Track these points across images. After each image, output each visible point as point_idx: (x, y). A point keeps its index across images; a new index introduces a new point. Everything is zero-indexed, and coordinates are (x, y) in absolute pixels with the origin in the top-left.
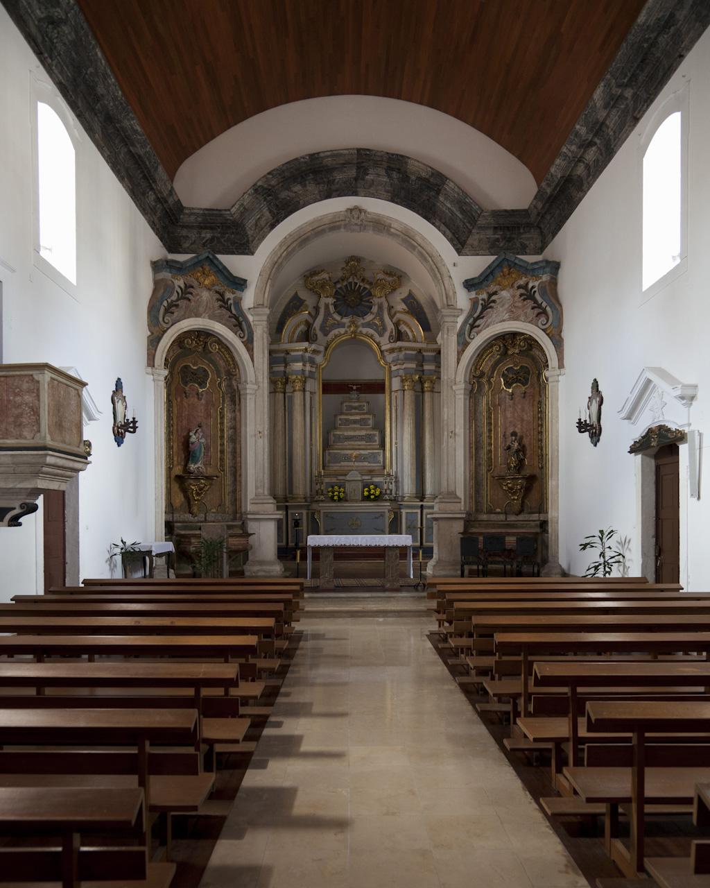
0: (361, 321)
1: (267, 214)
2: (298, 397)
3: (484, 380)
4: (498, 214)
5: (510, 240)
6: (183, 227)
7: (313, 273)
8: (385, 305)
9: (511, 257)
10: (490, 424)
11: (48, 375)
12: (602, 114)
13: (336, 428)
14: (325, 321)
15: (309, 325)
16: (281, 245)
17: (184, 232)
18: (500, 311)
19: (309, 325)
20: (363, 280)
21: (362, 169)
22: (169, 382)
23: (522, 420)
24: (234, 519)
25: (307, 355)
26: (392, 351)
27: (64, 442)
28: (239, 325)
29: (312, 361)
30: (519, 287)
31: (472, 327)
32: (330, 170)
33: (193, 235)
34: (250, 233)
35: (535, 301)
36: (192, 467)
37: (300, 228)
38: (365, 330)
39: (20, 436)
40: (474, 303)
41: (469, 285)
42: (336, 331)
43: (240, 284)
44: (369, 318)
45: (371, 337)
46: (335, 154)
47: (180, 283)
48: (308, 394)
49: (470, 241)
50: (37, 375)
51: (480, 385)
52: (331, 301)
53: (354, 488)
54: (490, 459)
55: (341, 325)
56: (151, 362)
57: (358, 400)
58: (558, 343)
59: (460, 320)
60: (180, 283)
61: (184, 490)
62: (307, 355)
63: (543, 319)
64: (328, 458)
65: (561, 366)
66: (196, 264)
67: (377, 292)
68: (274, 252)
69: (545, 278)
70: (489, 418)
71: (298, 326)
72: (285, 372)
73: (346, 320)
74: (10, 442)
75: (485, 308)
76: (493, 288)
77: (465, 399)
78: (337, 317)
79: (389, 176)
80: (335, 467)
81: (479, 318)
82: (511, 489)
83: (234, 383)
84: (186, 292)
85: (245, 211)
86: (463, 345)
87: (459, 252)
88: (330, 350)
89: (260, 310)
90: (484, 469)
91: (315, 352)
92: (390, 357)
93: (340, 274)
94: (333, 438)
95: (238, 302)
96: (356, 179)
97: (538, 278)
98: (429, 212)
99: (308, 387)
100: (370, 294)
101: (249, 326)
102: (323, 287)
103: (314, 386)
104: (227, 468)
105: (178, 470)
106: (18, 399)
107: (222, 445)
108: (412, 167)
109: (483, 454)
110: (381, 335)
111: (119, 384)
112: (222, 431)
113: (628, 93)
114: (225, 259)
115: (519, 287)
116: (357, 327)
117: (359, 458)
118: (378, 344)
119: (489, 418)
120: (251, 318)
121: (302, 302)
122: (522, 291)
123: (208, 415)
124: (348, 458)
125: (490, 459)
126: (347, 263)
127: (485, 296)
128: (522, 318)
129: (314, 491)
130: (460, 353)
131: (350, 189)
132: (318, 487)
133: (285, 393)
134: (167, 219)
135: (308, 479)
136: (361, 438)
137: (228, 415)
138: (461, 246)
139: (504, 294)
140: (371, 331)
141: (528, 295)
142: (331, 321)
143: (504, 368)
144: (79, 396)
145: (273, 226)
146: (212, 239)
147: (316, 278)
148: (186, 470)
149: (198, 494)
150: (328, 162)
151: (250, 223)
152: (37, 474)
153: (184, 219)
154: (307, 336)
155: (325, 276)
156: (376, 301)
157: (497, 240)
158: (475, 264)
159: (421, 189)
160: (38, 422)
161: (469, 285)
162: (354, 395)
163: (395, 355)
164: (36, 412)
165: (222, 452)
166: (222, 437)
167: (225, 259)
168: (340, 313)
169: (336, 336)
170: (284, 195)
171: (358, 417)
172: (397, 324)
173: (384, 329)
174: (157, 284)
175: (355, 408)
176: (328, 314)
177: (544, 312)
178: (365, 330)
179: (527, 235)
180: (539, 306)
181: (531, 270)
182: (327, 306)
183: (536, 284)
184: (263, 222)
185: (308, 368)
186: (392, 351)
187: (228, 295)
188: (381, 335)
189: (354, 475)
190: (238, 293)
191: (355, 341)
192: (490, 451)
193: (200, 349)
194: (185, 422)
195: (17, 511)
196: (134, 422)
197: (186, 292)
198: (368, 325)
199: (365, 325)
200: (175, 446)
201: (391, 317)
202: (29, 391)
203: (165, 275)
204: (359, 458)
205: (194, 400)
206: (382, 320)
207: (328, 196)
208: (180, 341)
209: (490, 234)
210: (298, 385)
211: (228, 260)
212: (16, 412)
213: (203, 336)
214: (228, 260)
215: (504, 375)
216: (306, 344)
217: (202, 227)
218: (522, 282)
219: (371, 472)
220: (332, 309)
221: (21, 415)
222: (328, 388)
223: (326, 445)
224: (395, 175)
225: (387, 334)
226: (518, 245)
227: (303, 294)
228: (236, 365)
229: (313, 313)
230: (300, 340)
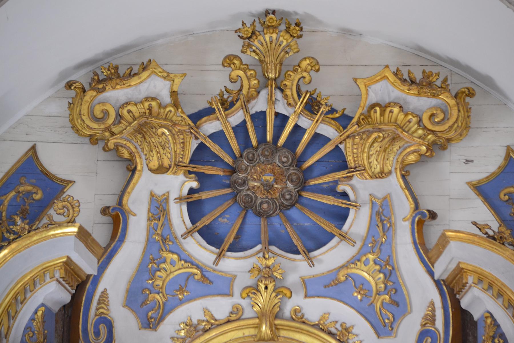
0: (297, 269)
8: (403, 207)
20: (312, 107)
38: (315, 308)
42: (193, 310)
44: (332, 256)
52: (177, 184)
55: (209, 283)
93: (217, 81)
100: (338, 162)
102: (143, 130)
121: (54, 188)
142: (172, 270)
147: (116, 94)
155: (156, 86)
156: (361, 188)
168: (211, 236)
172: (451, 288)
173: (398, 302)
176: (161, 239)
178: (315, 308)
182: (159, 208)
198: (331, 286)
199: (311, 288)
201: (427, 255)
206: (389, 270)
220: (179, 217)
227: (62, 158)
229: (101, 234)
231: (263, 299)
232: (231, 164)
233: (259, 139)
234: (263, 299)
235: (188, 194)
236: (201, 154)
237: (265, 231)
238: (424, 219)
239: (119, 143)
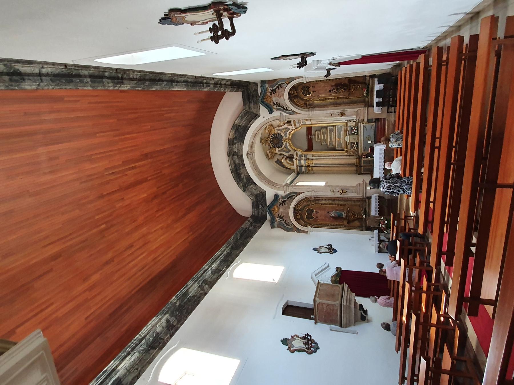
0: (284, 137)
1: (252, 186)
2: (314, 162)
3: (308, 103)
4: (244, 104)
5: (253, 96)
6: (258, 214)
7: (267, 156)
8: (277, 128)
9: (260, 99)
10: (326, 99)
11: (317, 299)
12: (212, 86)
13: (327, 144)
14: (284, 151)
15: (287, 157)
16: (262, 181)
17: (260, 214)
18: (281, 101)
19: (287, 157)
20: (269, 137)
21: (235, 154)
22: (313, 226)
23: (324, 86)
24: (365, 201)
25: (298, 158)
26: (295, 125)
27: (338, 294)
28: (291, 197)
29: (300, 156)
30: (271, 95)
31: (287, 110)
32: (235, 165)
33: (261, 211)
34: (258, 192)
35: (276, 88)
36: (344, 216)
37: (256, 174)
38: (288, 136)
39: (337, 310)
40: (277, 109)
41: (271, 112)
42: (289, 147)
43: (276, 196)
44: (283, 134)
45: (290, 133)
46: (230, 164)
47: (278, 219)
48: (313, 158)
49: (255, 112)
50: (317, 303)
51: (309, 105)
52: (277, 149)
53: (353, 139)
54: (341, 98)
55: (286, 146)
56: (306, 232)
57: (315, 135)
58: (293, 79)
59: (284, 114)
60: (278, 219)
61: (354, 220)
62: (298, 158)
63: (283, 85)
64: (339, 149)
65: (302, 77)
66: (271, 213)
67: (273, 132)
68: (265, 184)
69: (267, 86)
70: (323, 100)
71: (287, 162)
72: (305, 166)
73: (284, 143)
74: (339, 313)
75: (279, 106)
76: (272, 104)
77: (316, 111)
78: (283, 147)
79: (235, 144)
80: (343, 145)
81: (283, 107)
82: (354, 90)
83: (312, 199)
84: (281, 217)
85: (252, 194)
86: (294, 112)
87: (259, 116)
88: (296, 149)
89: (285, 189)
90: (346, 100)
91: (297, 156)
92: (298, 125)
93: (267, 146)
94: (331, 146)
95: (283, 197)
96: (237, 155)
97: (267, 89)
98: (246, 129)
99: (311, 158)
100: (274, 134)
101: (290, 193)
102: (272, 153)
103: (310, 155)
104: (345, 203)
105: (345, 223)
106: (325, 309)
107: (335, 204)
108: (231, 136)
109: (338, 101)
110: (289, 129)
111: (315, 249)
112: (330, 204)
113: (205, 81)
114: (268, 204)
115: (271, 95)
116: (286, 139)
117: (339, 137)
118: (293, 130)
119: (323, 100)
120: (288, 192)
121: (278, 160)
122: (272, 94)
123: (324, 209)
124: (339, 141)
125: (341, 98)
126: (263, 144)
127: (275, 106)
128: (283, 93)
129: (354, 154)
130: (297, 113)
131: (241, 157)
132: (352, 153)
133: (313, 166)
134: (258, 220)
135: (348, 157)
136: (331, 134)
137: (324, 202)
138: (256, 116)
139: (274, 100)
140: (288, 133)
141: (274, 91)
142: (285, 149)
143: (302, 96)
144: (323, 284)
145: (256, 184)
146: (262, 205)
147: (269, 155)
148: (345, 219)
149: (355, 215)
150: (233, 166)
151: (256, 192)
152: (349, 307)
153: (256, 214)
154: (291, 158)
155: (268, 151)
156: (276, 132)
157: (253, 101)
158: (263, 111)
159: (239, 132)
160: (332, 305)
161: (271, 112)
162: (313, 137)
163: (296, 124)
164: (329, 305)
165: (338, 205)
166: (332, 204)
167: (268, 204)
168: (282, 146)
169: (290, 147)
170: (245, 181)
171: (322, 136)
172: (285, 124)
173: (287, 128)
174: (278, 227)
175: (318, 136)
176: (282, 150)
177: (280, 85)
178: (288, 136)
179: (251, 89)
180: (278, 87)
181: (264, 91)
182: (279, 151)
183: (269, 89)
184: (254, 188)
185: (303, 158)
186: (295, 125)
187: (280, 201)
188: (289, 129)
189: (347, 139)
190: (280, 197)
191: (292, 139)
192: (337, 98)
193: (300, 212)
194: (327, 219)
195: (362, 312)
196: (328, 245)
197: (281, 217)
198: (285, 134)
199: (286, 136)
200: (336, 223)
201: (281, 126)
202: (322, 305)
203: (275, 224)
204: (339, 137)
205: (318, 215)
206: (283, 129)
207: (244, 165)
208: (297, 220)
209: (251, 105)
210: (310, 162)
211: (269, 201)
212: (329, 310)
213: (295, 211)
214: (269, 201)
215: (306, 95)
216: (294, 160)
217: (258, 208)
218: (269, 94)
219: (346, 131)
220: (280, 149)
221: (330, 309)
222: (310, 148)
223: (334, 149)
224: (235, 142)
225: (289, 127)
226: (254, 93)
227: (276, 160)
228: (305, 198)
229: (282, 156)
230: (293, 161)
231: (287, 141)
232: (485, 306)
233: (272, 142)
234: (287, 141)
235: (224, 93)
236: (274, 147)
237: (51, 172)
238: (279, 126)
239: (274, 155)
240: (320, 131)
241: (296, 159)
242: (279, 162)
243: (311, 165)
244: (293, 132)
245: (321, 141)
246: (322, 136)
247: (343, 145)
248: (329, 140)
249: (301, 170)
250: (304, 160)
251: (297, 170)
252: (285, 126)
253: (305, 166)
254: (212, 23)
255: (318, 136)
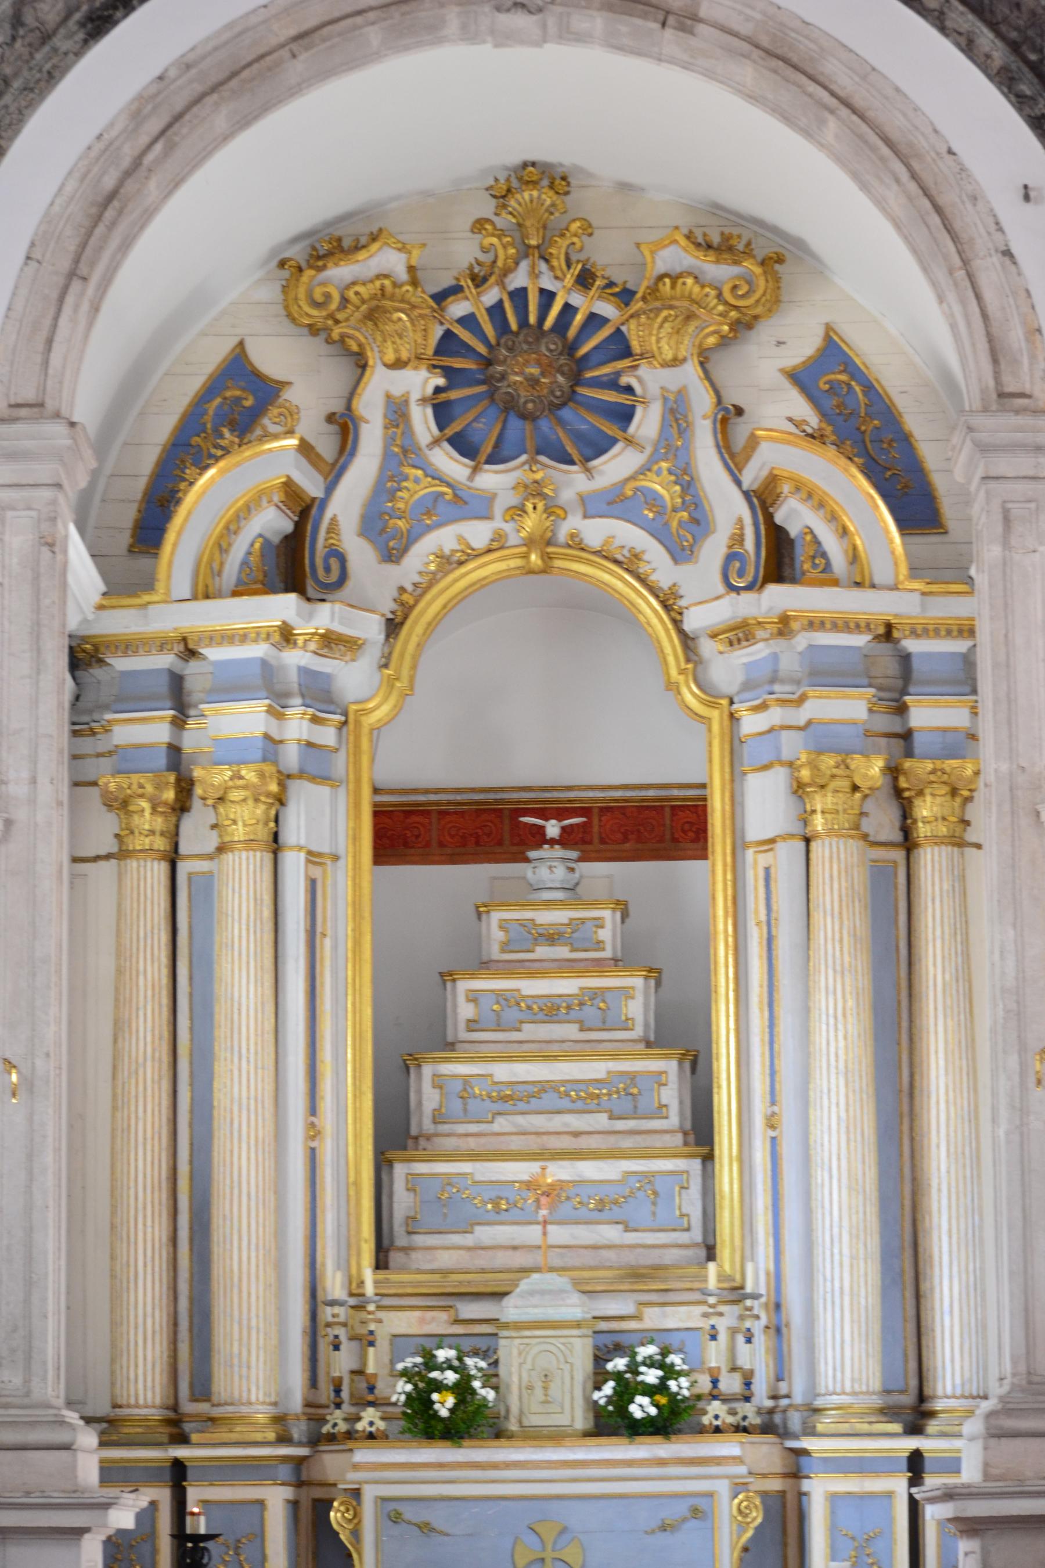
0: (573, 483)
2: (242, 877)
7: (328, 246)
8: (702, 402)
15: (304, 511)
20: (585, 280)
25: (295, 658)
26: (740, 633)
38: (596, 531)
42: (445, 538)
44: (616, 466)
45: (631, 564)
48: (294, 864)
52: (419, 382)
53: (545, 1372)
55: (463, 504)
62: (295, 658)
64: (402, 1202)
72: (174, 750)
73: (494, 480)
78: (450, 464)
80: (440, 1254)
91: (331, 642)
92: (727, 667)
93: (465, 252)
99: (294, 831)
100: (620, 347)
103: (328, 821)
110: (681, 552)
126: (503, 196)
136: (584, 1097)
140: (628, 535)
142: (416, 488)
154: (293, 564)
155: (388, 260)
156: (649, 380)
168: (464, 446)
169: (448, 562)
171: (567, 986)
172: (763, 500)
175: (552, 938)
176: (401, 452)
178: (596, 531)
182: (397, 413)
185: (297, 726)
186: (740, 633)
188: (681, 552)
198: (615, 502)
199: (589, 507)
201: (734, 459)
206: (687, 480)
210: (245, 818)
216: (284, 606)
219: (642, 1277)
220: (423, 423)
223: (395, 1134)
225: (714, 550)
227: (277, 355)
233: (519, 323)
234: (530, 523)
236: (448, 344)
238: (728, 415)
239: (345, 336)
240: (617, 963)
241: (286, 635)
242: (236, 403)
243: (196, 833)
244: (649, 608)
245: (485, 967)
246: (567, 986)
247: (440, 1254)
248: (503, 1072)
249: (132, 698)
250: (272, 743)
251: (128, 646)
252: (729, 508)
253: (174, 750)
254: (378, 283)
255: (552, 938)
